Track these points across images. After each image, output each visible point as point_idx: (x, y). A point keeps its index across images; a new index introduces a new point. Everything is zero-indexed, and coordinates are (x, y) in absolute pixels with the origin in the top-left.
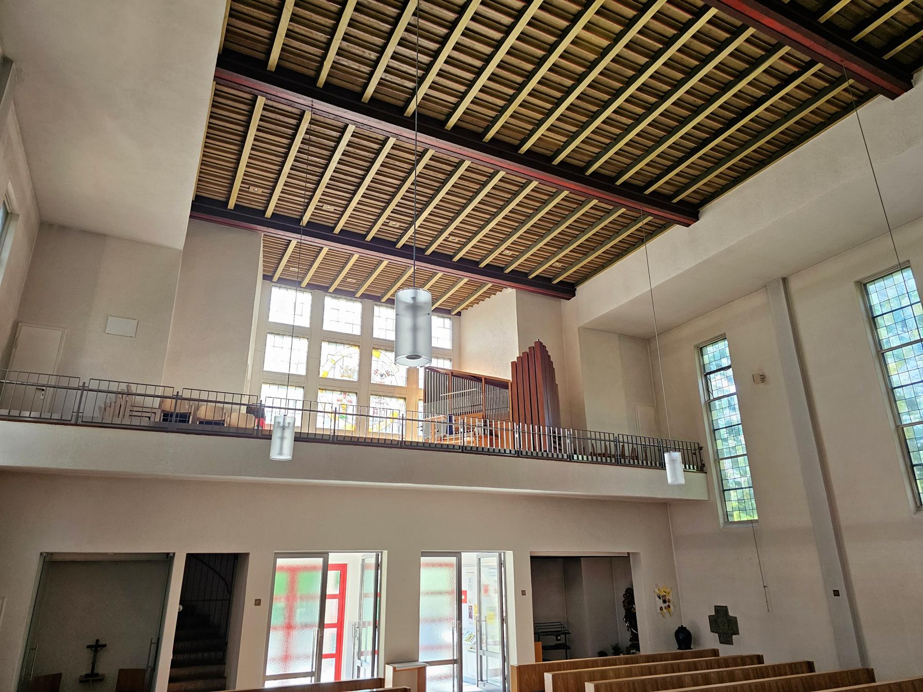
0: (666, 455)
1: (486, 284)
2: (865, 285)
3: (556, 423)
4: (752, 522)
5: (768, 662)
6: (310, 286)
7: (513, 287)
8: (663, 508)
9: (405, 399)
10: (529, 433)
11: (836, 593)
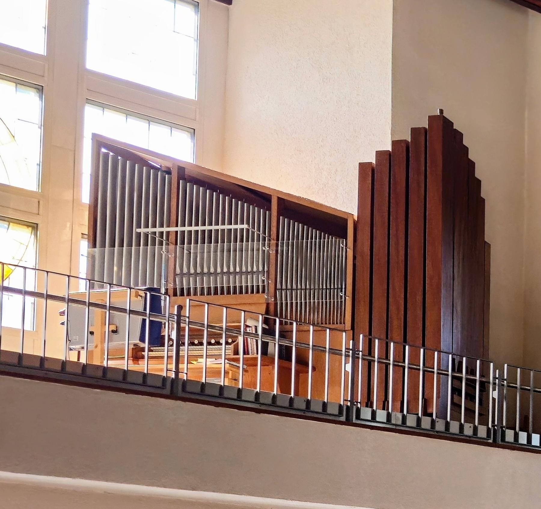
9: (35, 227)
10: (414, 370)
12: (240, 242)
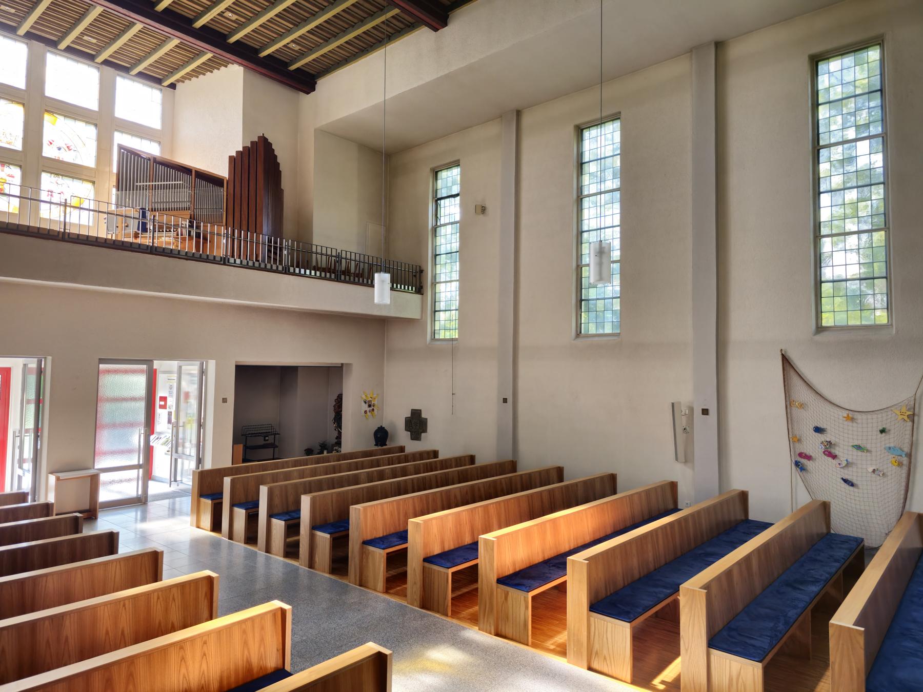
0: (376, 275)
1: (204, 53)
2: (582, 130)
3: (277, 231)
4: (452, 340)
5: (441, 456)
6: (29, 36)
7: (240, 64)
8: (378, 325)
9: (93, 183)
10: (252, 242)
11: (505, 400)
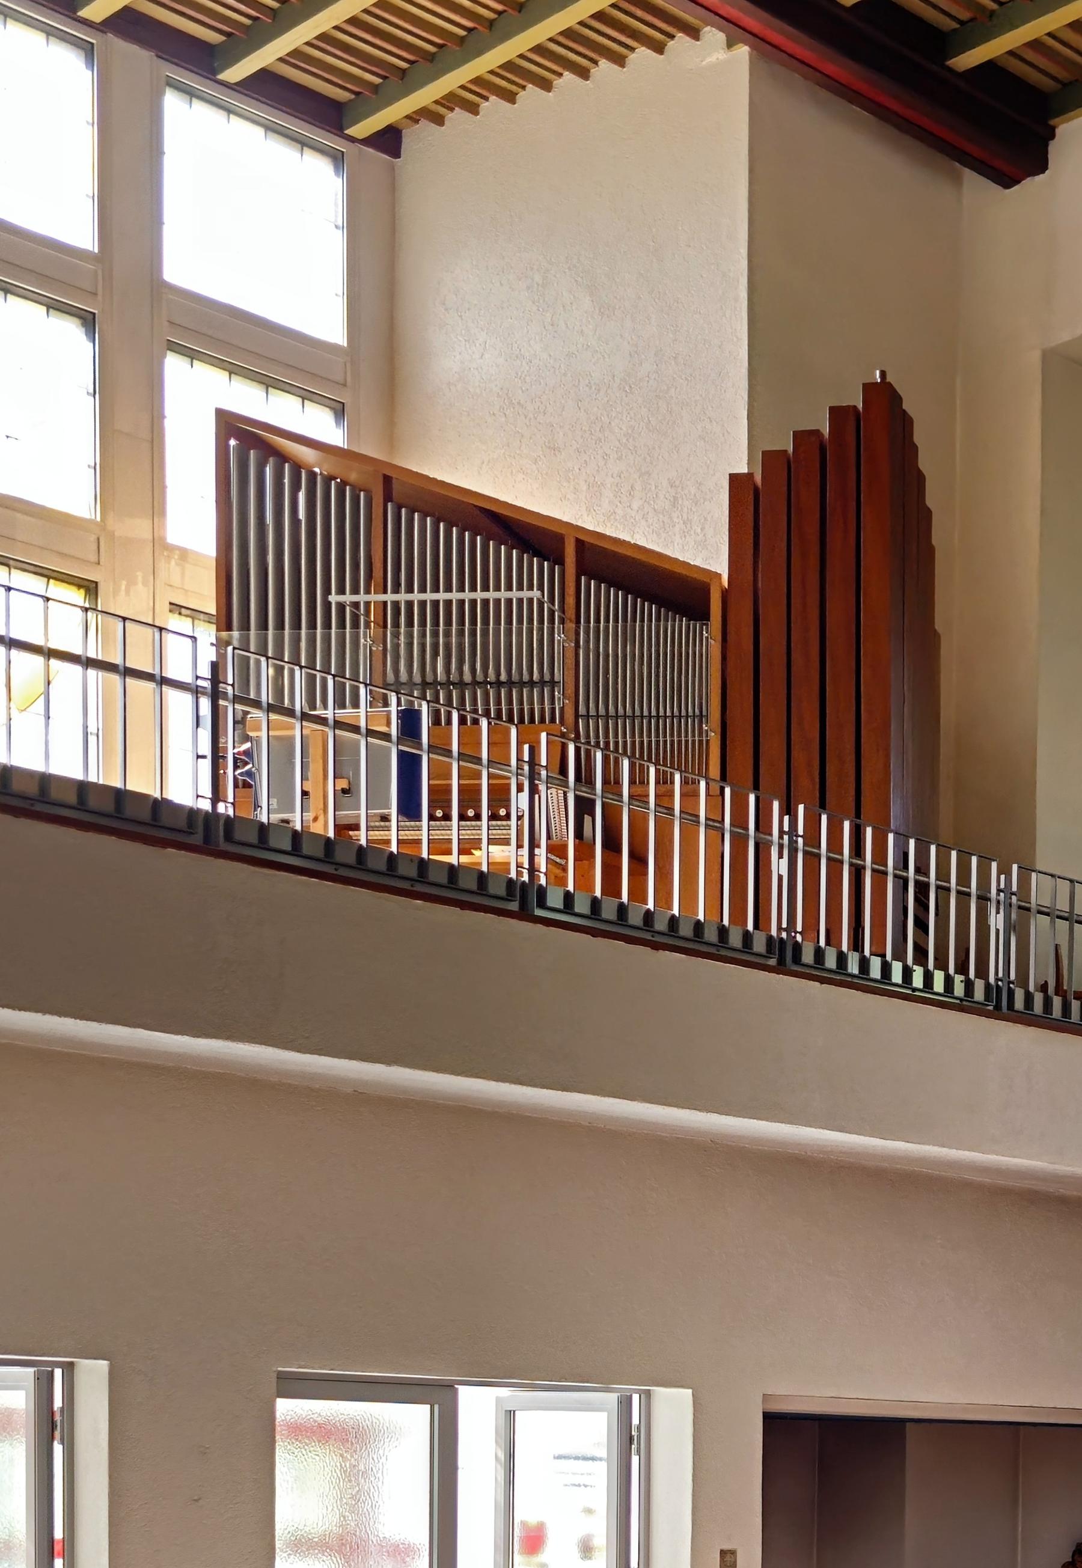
12: (337, 628)
